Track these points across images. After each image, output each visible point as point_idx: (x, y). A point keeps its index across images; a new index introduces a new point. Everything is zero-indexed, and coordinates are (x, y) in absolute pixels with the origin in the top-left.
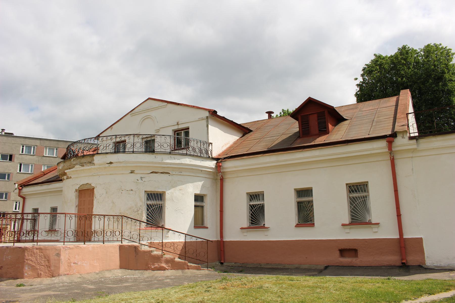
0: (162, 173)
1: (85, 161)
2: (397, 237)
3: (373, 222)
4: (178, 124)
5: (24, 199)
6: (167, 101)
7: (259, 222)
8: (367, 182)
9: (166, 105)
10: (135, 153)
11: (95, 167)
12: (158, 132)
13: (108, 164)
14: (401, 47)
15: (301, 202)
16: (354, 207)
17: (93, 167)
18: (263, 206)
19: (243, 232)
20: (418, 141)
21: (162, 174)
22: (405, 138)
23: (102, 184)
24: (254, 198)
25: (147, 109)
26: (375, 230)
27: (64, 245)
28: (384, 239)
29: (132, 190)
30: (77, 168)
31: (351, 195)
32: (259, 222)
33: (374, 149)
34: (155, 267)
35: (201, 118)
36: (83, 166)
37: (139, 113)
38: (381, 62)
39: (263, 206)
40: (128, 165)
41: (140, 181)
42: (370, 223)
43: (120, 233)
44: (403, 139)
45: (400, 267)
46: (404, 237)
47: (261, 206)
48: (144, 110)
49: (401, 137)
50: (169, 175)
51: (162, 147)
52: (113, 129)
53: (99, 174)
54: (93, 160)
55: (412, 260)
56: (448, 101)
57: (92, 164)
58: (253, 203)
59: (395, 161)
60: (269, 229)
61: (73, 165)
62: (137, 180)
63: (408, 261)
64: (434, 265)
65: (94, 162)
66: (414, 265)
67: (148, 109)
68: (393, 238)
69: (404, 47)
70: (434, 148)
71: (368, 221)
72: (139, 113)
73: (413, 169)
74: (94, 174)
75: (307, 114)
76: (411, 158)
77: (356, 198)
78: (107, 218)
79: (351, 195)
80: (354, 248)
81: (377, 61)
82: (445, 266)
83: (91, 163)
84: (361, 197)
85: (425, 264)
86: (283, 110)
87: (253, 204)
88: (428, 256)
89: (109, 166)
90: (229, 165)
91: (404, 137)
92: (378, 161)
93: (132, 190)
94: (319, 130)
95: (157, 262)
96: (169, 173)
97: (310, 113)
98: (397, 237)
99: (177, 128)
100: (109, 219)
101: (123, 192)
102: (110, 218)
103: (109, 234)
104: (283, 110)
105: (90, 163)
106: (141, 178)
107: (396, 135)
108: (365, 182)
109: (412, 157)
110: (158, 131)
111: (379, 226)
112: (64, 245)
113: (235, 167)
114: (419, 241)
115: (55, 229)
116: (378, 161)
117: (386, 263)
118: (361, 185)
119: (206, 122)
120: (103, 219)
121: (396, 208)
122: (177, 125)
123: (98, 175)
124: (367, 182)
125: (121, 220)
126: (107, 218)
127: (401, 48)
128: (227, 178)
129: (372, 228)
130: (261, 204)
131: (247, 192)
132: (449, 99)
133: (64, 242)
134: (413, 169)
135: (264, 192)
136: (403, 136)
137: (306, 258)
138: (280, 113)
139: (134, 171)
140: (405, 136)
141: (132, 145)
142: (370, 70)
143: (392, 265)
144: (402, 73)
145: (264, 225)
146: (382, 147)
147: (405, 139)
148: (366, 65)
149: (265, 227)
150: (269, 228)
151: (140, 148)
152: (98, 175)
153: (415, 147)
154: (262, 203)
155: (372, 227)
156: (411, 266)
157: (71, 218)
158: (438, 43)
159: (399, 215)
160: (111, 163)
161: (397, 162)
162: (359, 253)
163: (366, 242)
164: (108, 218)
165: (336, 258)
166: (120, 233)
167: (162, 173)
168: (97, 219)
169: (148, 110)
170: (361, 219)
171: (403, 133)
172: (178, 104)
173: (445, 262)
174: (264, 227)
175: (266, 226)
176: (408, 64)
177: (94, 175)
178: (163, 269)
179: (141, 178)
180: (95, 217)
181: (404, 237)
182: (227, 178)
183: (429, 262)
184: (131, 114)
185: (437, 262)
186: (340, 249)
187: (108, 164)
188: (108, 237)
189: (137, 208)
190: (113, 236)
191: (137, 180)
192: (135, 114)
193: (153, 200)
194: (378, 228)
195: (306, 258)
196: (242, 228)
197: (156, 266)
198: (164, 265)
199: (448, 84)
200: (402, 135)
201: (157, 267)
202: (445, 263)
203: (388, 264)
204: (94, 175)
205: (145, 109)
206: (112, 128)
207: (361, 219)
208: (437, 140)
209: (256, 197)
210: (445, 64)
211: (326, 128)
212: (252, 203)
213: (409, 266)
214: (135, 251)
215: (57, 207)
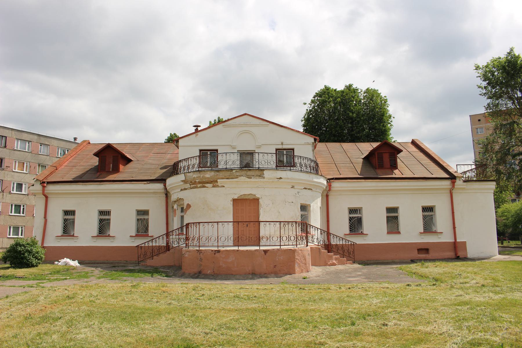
0: (309, 189)
1: (253, 174)
3: (438, 231)
4: (282, 144)
5: (47, 197)
6: (268, 121)
7: (102, 231)
9: (268, 124)
10: (291, 171)
11: (265, 180)
12: (260, 148)
13: (277, 179)
14: (348, 84)
15: (389, 217)
16: (426, 221)
17: (262, 180)
18: (360, 218)
19: (132, 239)
21: (309, 190)
23: (268, 196)
24: (353, 212)
25: (245, 124)
26: (112, 240)
27: (297, 247)
29: (293, 202)
30: (240, 179)
31: (424, 214)
32: (102, 231)
33: (442, 185)
34: (330, 263)
35: (307, 143)
36: (251, 178)
37: (234, 126)
39: (360, 218)
40: (293, 181)
41: (297, 195)
42: (435, 232)
43: (294, 238)
45: (456, 259)
46: (457, 241)
47: (359, 218)
48: (241, 124)
50: (312, 191)
51: (269, 164)
52: (198, 135)
53: (264, 187)
54: (263, 174)
55: (461, 254)
57: (261, 177)
58: (352, 215)
60: (78, 237)
61: (236, 176)
62: (296, 194)
65: (264, 176)
66: (462, 257)
67: (247, 124)
69: (350, 86)
72: (234, 126)
74: (260, 187)
75: (381, 152)
77: (427, 215)
78: (290, 224)
79: (424, 214)
80: (427, 248)
82: (476, 257)
83: (261, 176)
86: (219, 118)
87: (352, 216)
89: (278, 180)
90: (336, 185)
93: (293, 202)
94: (391, 165)
95: (331, 260)
96: (311, 189)
97: (384, 152)
98: (452, 240)
99: (282, 147)
100: (284, 225)
101: (286, 203)
102: (285, 224)
103: (284, 238)
104: (219, 118)
105: (260, 176)
106: (298, 192)
110: (260, 147)
112: (297, 247)
113: (341, 187)
114: (464, 243)
119: (311, 147)
120: (295, 225)
122: (281, 145)
123: (263, 187)
125: (198, 226)
126: (290, 224)
128: (331, 195)
130: (359, 217)
131: (349, 207)
133: (280, 246)
135: (400, 211)
137: (396, 255)
138: (215, 120)
139: (294, 186)
140: (460, 180)
141: (225, 162)
142: (325, 100)
145: (74, 234)
150: (115, 236)
151: (224, 165)
152: (263, 187)
154: (359, 216)
157: (292, 225)
158: (376, 89)
159: (454, 228)
160: (281, 178)
161: (453, 194)
162: (430, 251)
163: (435, 244)
164: (284, 224)
165: (415, 255)
166: (294, 238)
167: (309, 189)
168: (290, 225)
169: (246, 125)
170: (428, 228)
172: (282, 126)
174: (362, 233)
175: (75, 235)
177: (259, 187)
178: (334, 264)
179: (298, 192)
180: (288, 223)
181: (457, 241)
182: (331, 195)
183: (469, 256)
184: (223, 125)
186: (418, 248)
187: (277, 179)
188: (292, 242)
189: (296, 217)
190: (289, 240)
191: (296, 194)
192: (229, 126)
193: (354, 214)
195: (396, 255)
196: (131, 236)
197: (331, 262)
198: (334, 261)
201: (331, 263)
204: (259, 187)
205: (243, 124)
206: (198, 134)
207: (428, 228)
209: (355, 211)
211: (395, 164)
212: (351, 216)
214: (319, 251)
215: (111, 210)
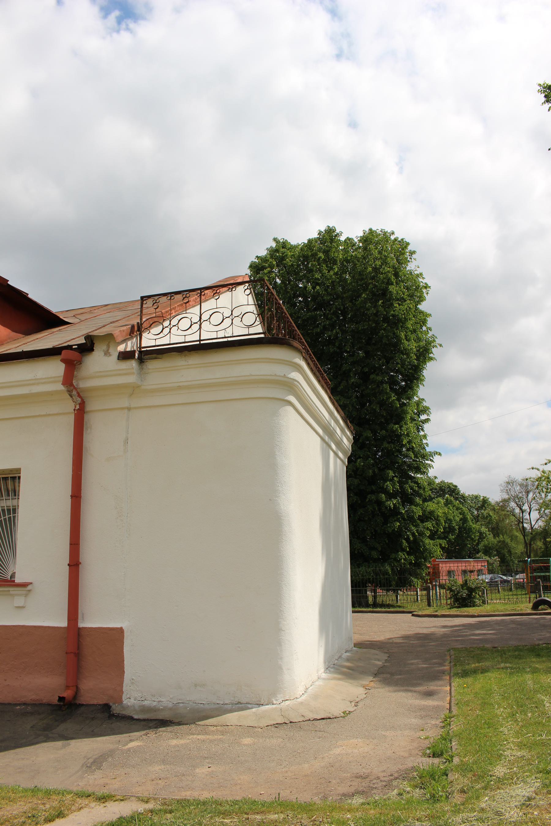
2: (63, 623)
8: (18, 471)
20: (144, 367)
22: (110, 355)
26: (19, 601)
28: (35, 627)
38: (283, 254)
44: (106, 358)
49: (104, 351)
56: (393, 337)
59: (86, 417)
60: (29, 587)
63: (82, 691)
64: (146, 703)
68: (56, 626)
70: (180, 388)
71: (11, 578)
73: (126, 441)
76: (126, 411)
81: (277, 251)
84: (7, 509)
85: (121, 702)
88: (133, 678)
91: (110, 351)
92: (49, 415)
98: (63, 623)
107: (92, 345)
108: (11, 471)
109: (129, 409)
111: (30, 591)
115: (13, 575)
116: (49, 415)
117: (30, 697)
118: (8, 477)
121: (71, 544)
124: (18, 471)
127: (324, 232)
129: (13, 595)
132: (394, 333)
134: (126, 441)
136: (108, 350)
142: (260, 266)
143: (44, 701)
144: (316, 276)
146: (54, 377)
147: (111, 358)
148: (257, 257)
149: (14, 581)
150: (31, 583)
153: (132, 379)
155: (11, 592)
156: (87, 705)
171: (109, 342)
173: (171, 696)
176: (330, 261)
185: (153, 696)
194: (26, 596)
199: (395, 305)
200: (105, 347)
202: (171, 698)
203: (34, 697)
208: (188, 365)
210: (394, 267)
213: (83, 705)
